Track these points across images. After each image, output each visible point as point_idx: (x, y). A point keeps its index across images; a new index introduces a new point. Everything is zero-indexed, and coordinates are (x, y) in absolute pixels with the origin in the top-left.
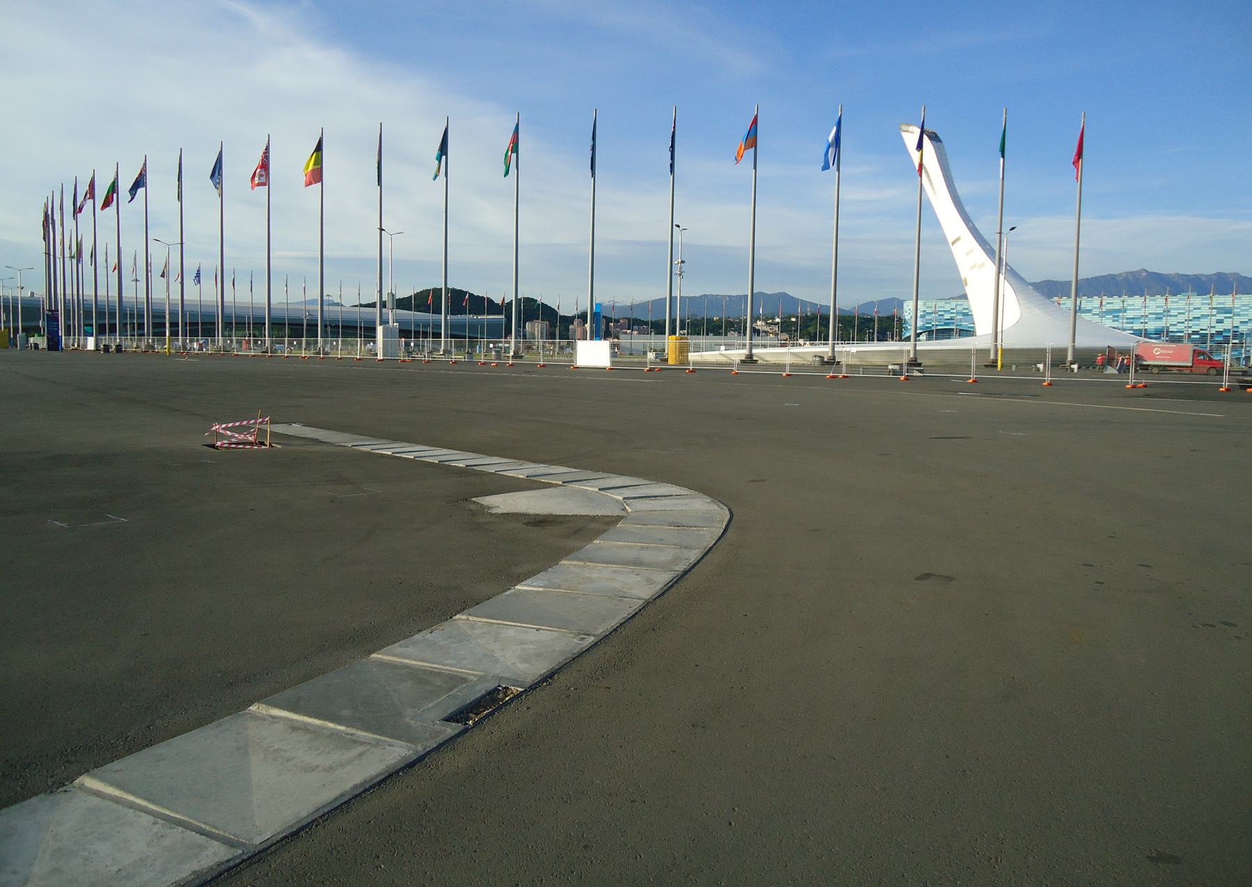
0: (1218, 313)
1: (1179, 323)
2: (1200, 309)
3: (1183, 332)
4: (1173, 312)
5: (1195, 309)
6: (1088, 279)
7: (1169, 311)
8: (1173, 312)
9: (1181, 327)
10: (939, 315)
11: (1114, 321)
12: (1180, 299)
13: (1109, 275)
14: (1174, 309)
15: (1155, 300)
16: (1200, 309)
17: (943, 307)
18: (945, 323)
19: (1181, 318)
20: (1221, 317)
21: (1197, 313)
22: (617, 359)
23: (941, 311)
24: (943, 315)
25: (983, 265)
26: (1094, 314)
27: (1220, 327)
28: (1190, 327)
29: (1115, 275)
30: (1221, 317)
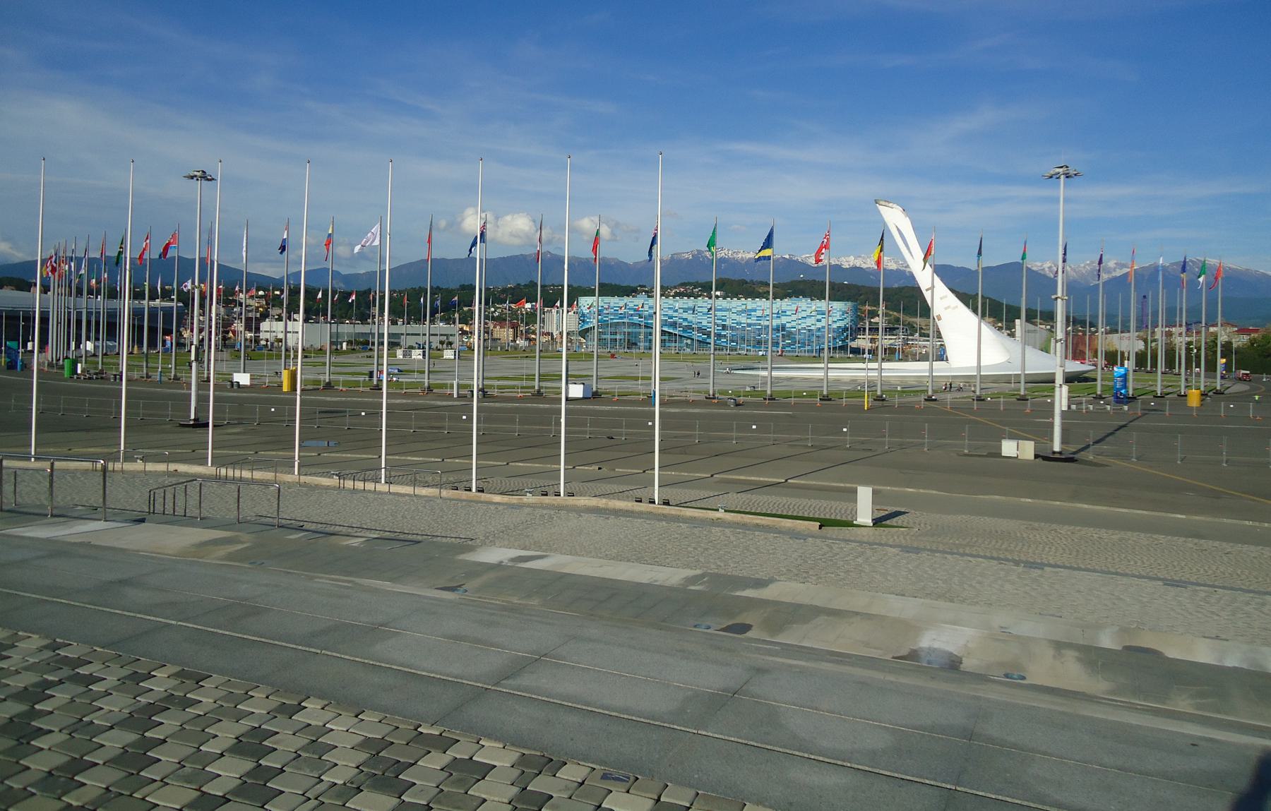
0: (818, 314)
1: (792, 321)
2: (805, 311)
3: (795, 328)
4: (543, 316)
5: (802, 311)
6: (504, 258)
7: (785, 312)
8: (788, 313)
9: (794, 324)
10: (615, 310)
11: (747, 318)
12: (793, 303)
13: (522, 255)
14: (789, 310)
15: (623, 300)
16: (805, 311)
17: (618, 303)
18: (620, 317)
19: (794, 317)
20: (819, 317)
21: (804, 314)
22: (392, 340)
23: (615, 307)
24: (617, 310)
25: (957, 307)
26: (733, 313)
27: (819, 325)
28: (800, 324)
29: (526, 256)
30: (819, 317)
